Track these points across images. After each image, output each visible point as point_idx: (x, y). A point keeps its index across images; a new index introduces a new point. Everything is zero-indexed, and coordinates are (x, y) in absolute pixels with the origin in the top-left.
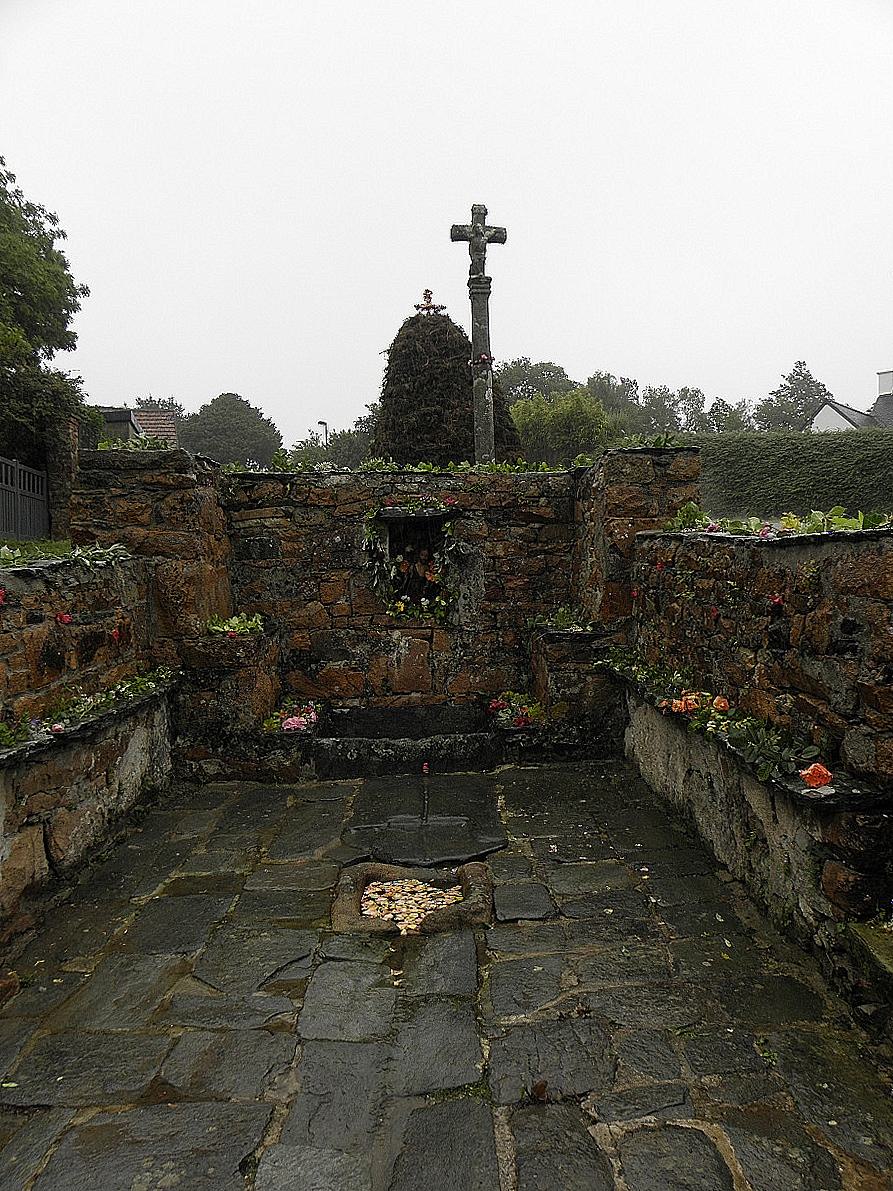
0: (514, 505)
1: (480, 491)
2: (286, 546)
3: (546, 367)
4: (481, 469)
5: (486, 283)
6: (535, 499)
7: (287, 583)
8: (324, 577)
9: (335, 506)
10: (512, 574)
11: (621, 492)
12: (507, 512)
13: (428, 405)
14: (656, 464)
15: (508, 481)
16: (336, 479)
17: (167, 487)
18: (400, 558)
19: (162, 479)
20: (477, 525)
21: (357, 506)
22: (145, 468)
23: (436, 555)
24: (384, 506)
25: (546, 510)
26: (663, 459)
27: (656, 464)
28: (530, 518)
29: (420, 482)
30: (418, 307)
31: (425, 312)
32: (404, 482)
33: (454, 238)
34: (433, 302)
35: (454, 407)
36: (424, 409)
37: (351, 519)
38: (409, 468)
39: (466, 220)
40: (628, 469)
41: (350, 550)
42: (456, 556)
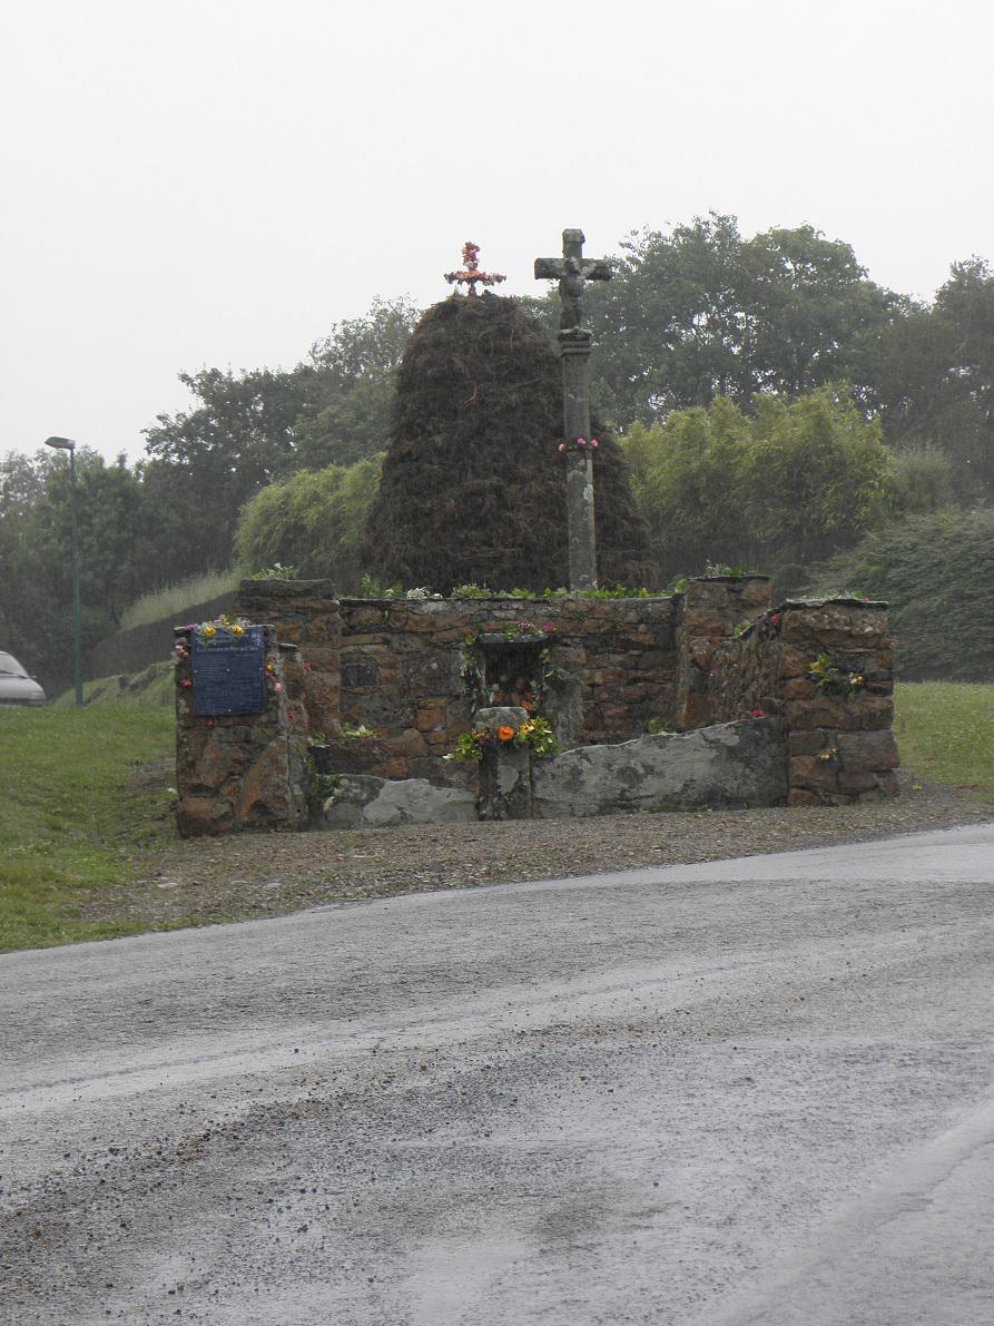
0: (613, 630)
1: (579, 617)
2: (384, 672)
3: (799, 243)
4: (583, 593)
5: (583, 339)
6: (633, 626)
7: (385, 709)
8: (422, 703)
9: (432, 633)
10: (612, 701)
11: (700, 615)
12: (607, 638)
13: (478, 476)
14: (730, 591)
15: (607, 608)
16: (432, 606)
17: (316, 611)
18: (496, 686)
19: (313, 604)
20: (576, 653)
21: (454, 633)
22: (299, 594)
23: (533, 684)
24: (481, 631)
25: (643, 635)
26: (737, 586)
27: (730, 591)
28: (627, 646)
29: (518, 609)
30: (451, 278)
31: (464, 289)
32: (500, 609)
33: (538, 275)
34: (480, 269)
35: (524, 480)
36: (472, 482)
37: (449, 646)
38: (503, 594)
39: (556, 252)
40: (706, 595)
41: (447, 676)
42: (554, 682)
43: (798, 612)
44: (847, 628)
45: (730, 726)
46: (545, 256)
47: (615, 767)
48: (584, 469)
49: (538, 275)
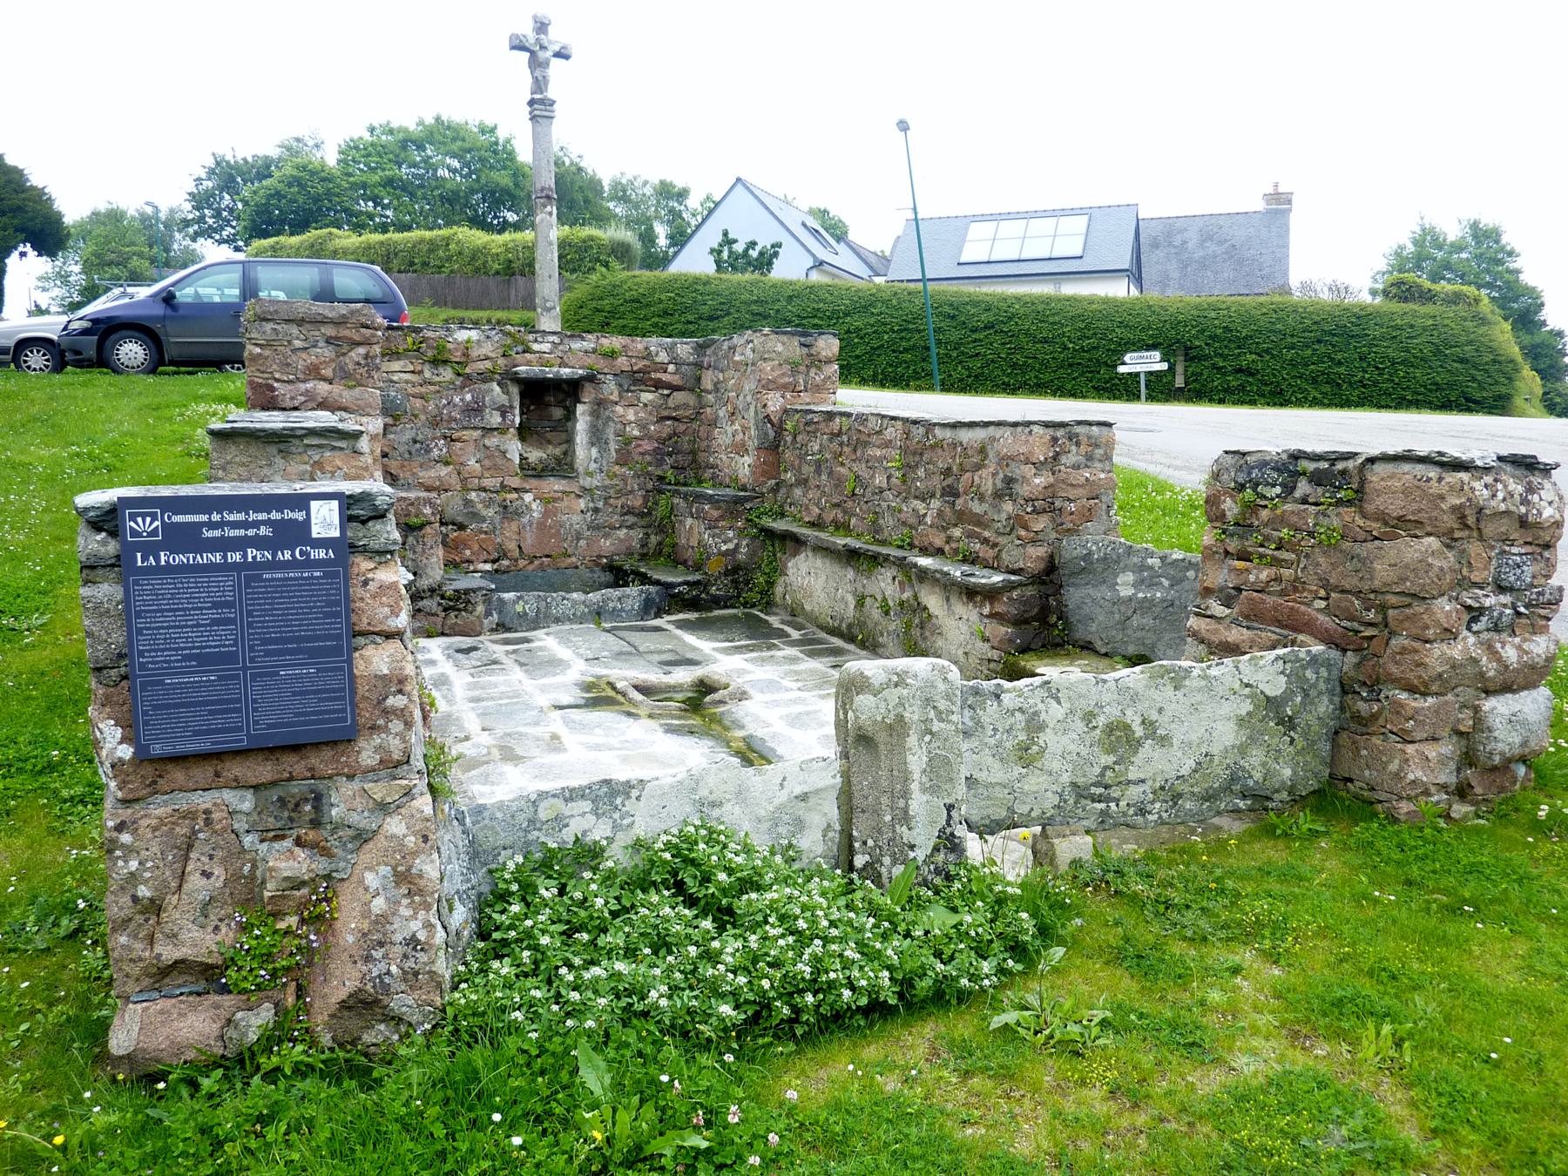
39: (527, 30)
43: (1464, 476)
44: (1523, 509)
45: (1278, 658)
46: (519, 32)
47: (1101, 721)
48: (550, 214)
49: (513, 48)
